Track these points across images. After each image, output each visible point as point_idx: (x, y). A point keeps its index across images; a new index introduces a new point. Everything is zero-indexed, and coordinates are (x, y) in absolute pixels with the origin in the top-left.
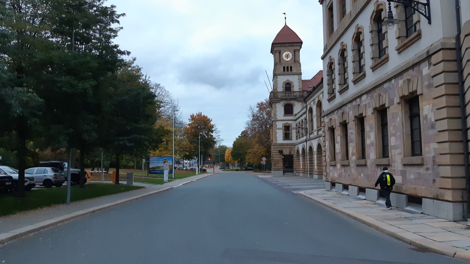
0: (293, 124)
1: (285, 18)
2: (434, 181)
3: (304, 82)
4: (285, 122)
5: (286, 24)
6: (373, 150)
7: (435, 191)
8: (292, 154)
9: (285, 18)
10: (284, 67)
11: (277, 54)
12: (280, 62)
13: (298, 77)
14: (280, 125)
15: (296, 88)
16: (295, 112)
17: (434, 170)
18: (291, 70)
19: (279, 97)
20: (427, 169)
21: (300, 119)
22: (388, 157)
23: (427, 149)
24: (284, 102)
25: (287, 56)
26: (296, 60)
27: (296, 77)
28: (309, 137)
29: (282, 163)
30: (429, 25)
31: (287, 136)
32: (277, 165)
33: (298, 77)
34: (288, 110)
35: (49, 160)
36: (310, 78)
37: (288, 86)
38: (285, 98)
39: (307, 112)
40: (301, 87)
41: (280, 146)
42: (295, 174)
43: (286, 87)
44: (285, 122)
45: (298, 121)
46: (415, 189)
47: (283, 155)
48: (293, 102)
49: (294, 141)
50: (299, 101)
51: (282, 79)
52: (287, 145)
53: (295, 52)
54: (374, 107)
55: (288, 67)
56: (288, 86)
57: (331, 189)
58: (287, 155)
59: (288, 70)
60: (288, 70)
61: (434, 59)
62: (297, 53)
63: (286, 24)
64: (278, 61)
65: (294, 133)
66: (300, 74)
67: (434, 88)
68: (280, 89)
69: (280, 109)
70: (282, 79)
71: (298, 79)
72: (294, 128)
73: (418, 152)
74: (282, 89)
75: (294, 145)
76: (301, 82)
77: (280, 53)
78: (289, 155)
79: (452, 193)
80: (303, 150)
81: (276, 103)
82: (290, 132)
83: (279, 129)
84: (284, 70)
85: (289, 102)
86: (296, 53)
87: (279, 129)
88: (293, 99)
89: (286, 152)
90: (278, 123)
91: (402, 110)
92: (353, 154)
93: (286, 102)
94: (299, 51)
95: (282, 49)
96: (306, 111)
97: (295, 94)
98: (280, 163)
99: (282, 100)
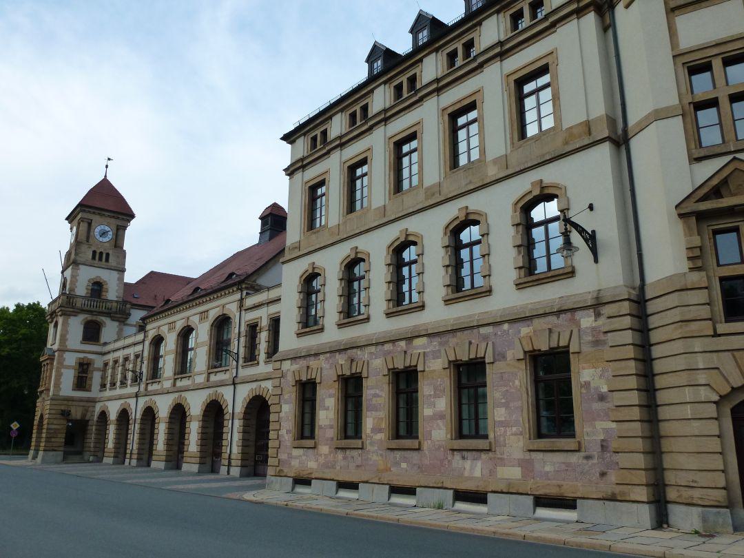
0: (98, 362)
1: (107, 166)
2: (603, 474)
3: (126, 284)
4: (81, 355)
5: (106, 176)
6: (442, 427)
7: (607, 487)
8: (87, 418)
9: (107, 166)
10: (94, 252)
11: (84, 226)
12: (88, 241)
13: (118, 276)
14: (71, 359)
15: (113, 293)
16: (102, 340)
17: (603, 459)
18: (107, 260)
19: (79, 305)
20: (588, 458)
21: (127, 351)
22: (361, 438)
23: (587, 429)
24: (86, 316)
25: (103, 234)
26: (118, 243)
27: (115, 274)
28: (146, 389)
29: (64, 435)
30: (595, 265)
31: (81, 382)
32: (53, 440)
33: (118, 276)
34: (92, 333)
35: (55, 387)
36: (134, 281)
37: (97, 288)
38: (88, 308)
39: (147, 343)
40: (121, 295)
41: (65, 402)
42: (86, 458)
43: (92, 290)
44: (81, 355)
45: (106, 358)
46: (560, 486)
47: (69, 421)
48: (103, 319)
49: (95, 392)
50: (113, 319)
51: (87, 274)
52: (81, 400)
53: (117, 230)
54: (452, 358)
55: (101, 253)
56: (97, 288)
57: (293, 489)
58: (77, 420)
59: (100, 259)
60: (100, 259)
61: (607, 310)
62: (120, 232)
63: (106, 176)
64: (83, 237)
65: (96, 378)
66: (123, 271)
67: (608, 348)
68: (82, 290)
69: (76, 326)
70: (87, 274)
71: (119, 279)
72: (98, 369)
73: (307, 433)
74: (85, 291)
75: (94, 401)
76: (123, 286)
77: (90, 224)
78: (80, 420)
79: (647, 489)
80: (124, 415)
81: (69, 315)
82: (89, 376)
83: (68, 367)
84: (94, 258)
85: (94, 318)
86: (120, 231)
87: (68, 367)
88: (102, 312)
89: (76, 413)
90: (67, 355)
91: (526, 369)
92: (376, 430)
93: (89, 317)
94: (125, 228)
95: (96, 218)
96: (144, 341)
97: (109, 305)
98: (60, 435)
99: (83, 311)
